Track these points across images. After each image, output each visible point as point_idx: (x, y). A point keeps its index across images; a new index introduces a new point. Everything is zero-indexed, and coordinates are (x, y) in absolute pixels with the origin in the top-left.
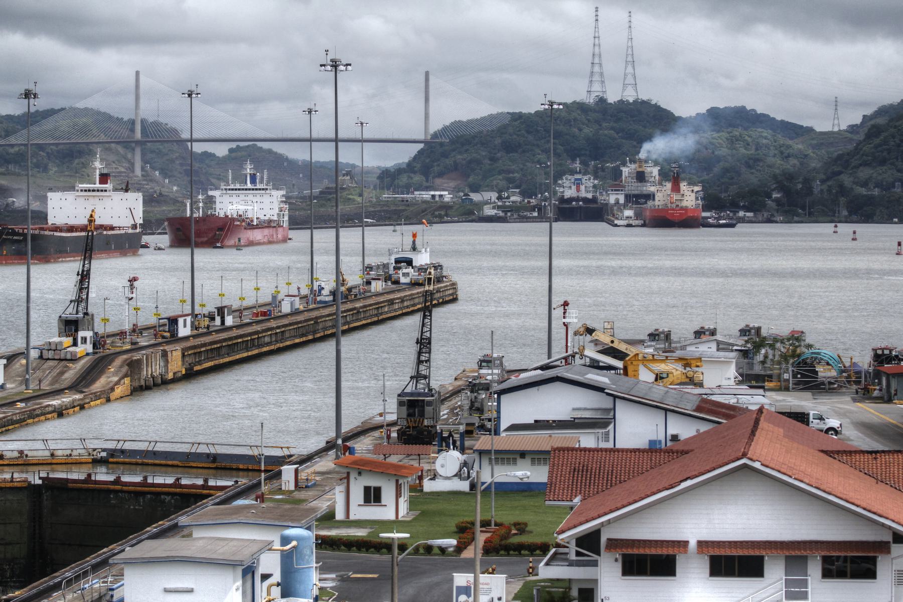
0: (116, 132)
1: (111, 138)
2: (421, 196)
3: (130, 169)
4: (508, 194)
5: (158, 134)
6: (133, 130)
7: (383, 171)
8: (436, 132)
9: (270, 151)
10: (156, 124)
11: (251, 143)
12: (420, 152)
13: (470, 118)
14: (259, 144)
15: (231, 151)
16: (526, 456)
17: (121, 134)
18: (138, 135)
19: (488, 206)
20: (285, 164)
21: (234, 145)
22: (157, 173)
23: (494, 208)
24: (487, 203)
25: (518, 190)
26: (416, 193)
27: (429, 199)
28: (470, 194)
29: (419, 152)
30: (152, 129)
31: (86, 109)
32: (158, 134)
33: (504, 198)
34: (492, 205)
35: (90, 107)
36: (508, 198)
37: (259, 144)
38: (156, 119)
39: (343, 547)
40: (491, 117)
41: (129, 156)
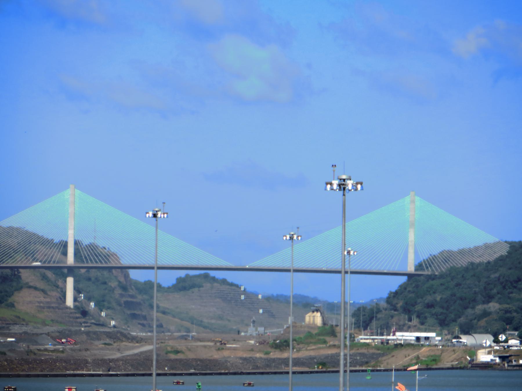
0: (45, 255)
1: (49, 262)
2: (404, 338)
3: (61, 299)
4: (507, 337)
5: (94, 259)
6: (65, 254)
7: (359, 309)
8: (421, 262)
9: (224, 282)
10: (92, 247)
11: (202, 272)
12: (403, 288)
13: (461, 247)
14: (212, 273)
15: (180, 280)
16: (394, 346)
17: (52, 257)
18: (71, 259)
19: (483, 351)
20: (243, 297)
21: (182, 273)
22: (92, 304)
23: (489, 353)
24: (482, 347)
25: (516, 333)
26: (398, 334)
27: (413, 342)
28: (462, 336)
29: (400, 286)
30: (87, 253)
31: (11, 228)
32: (94, 259)
33: (502, 342)
34: (487, 350)
35: (15, 225)
36: (506, 341)
37: (212, 273)
38: (92, 241)
39: (345, 362)
40: (487, 247)
41: (60, 283)
